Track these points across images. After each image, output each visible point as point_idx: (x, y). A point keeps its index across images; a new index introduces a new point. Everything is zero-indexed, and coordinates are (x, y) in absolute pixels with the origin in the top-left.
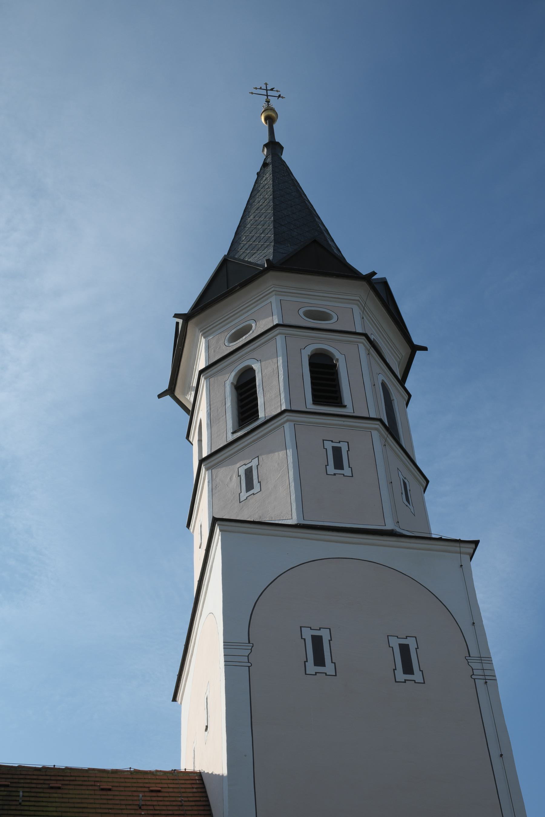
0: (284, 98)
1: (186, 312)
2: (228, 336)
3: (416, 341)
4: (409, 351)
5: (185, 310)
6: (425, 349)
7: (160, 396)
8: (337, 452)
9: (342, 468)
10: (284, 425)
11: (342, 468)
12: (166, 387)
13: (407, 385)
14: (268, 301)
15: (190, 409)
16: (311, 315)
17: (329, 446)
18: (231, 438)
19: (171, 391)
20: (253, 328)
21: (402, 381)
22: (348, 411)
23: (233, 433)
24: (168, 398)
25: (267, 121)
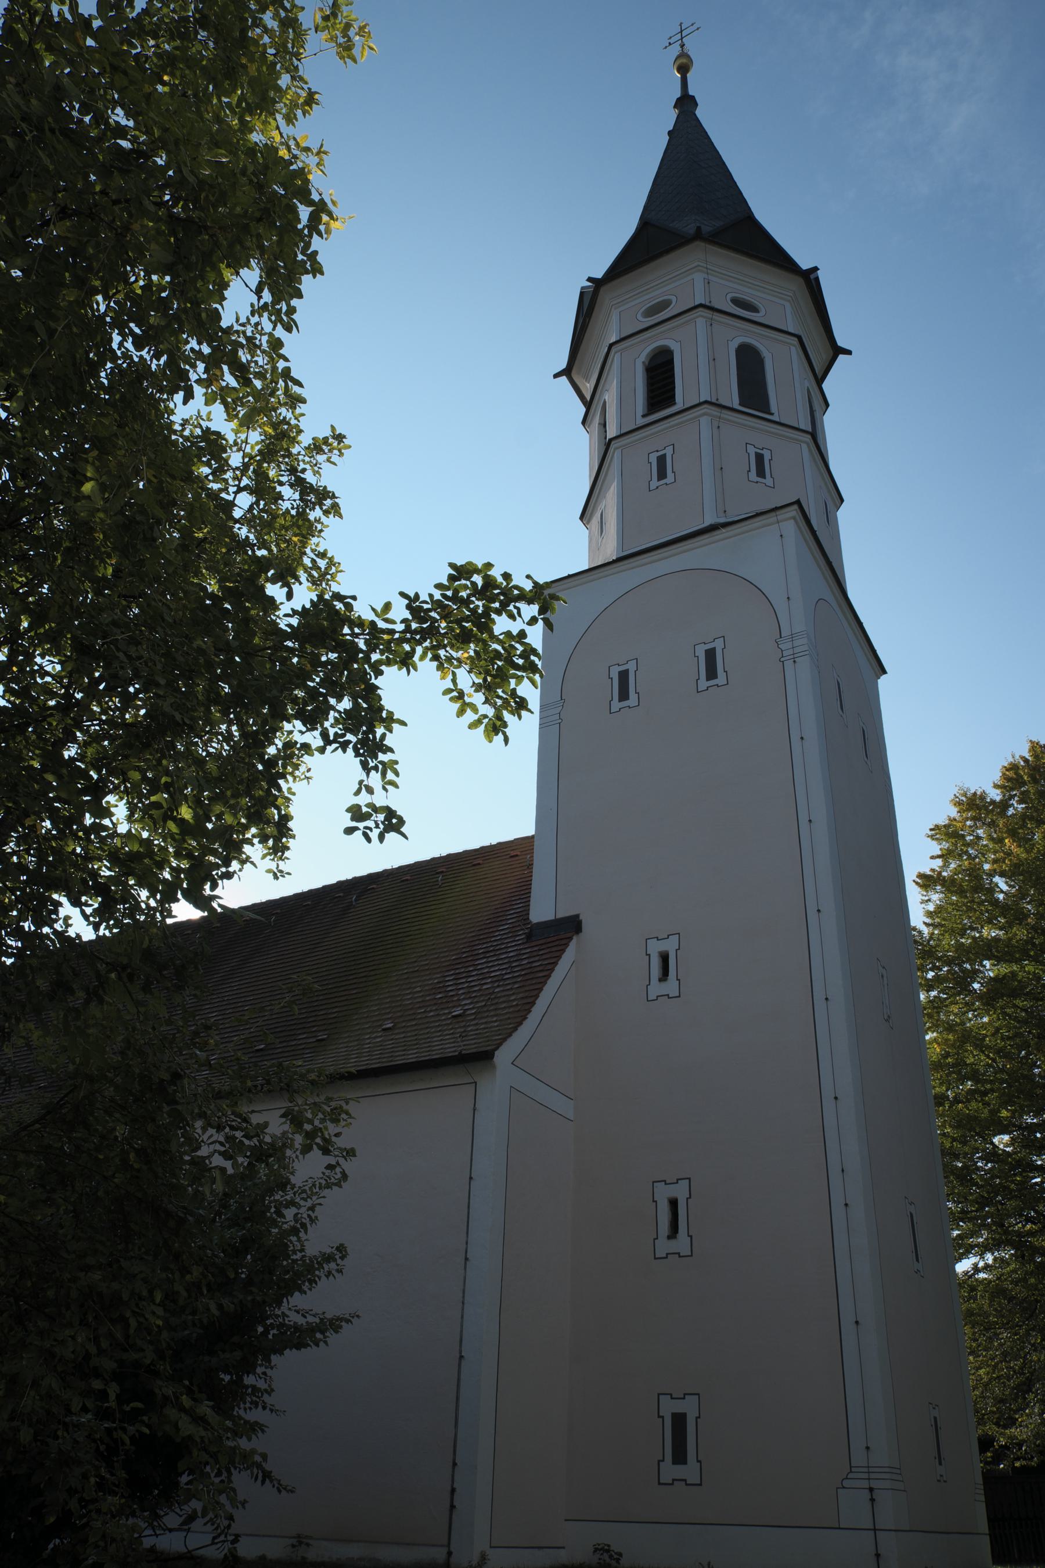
0: (332, 1337)
1: (600, 277)
2: (644, 308)
3: (841, 342)
4: (831, 353)
5: (599, 274)
6: (849, 352)
7: (556, 376)
8: (760, 458)
9: (764, 477)
10: (701, 419)
11: (764, 477)
12: (563, 365)
13: (824, 386)
14: (689, 278)
15: (588, 398)
16: (736, 301)
17: (752, 450)
18: (641, 421)
19: (567, 372)
20: (674, 303)
21: (820, 380)
22: (775, 418)
23: (644, 416)
24: (564, 379)
25: (610, 503)
